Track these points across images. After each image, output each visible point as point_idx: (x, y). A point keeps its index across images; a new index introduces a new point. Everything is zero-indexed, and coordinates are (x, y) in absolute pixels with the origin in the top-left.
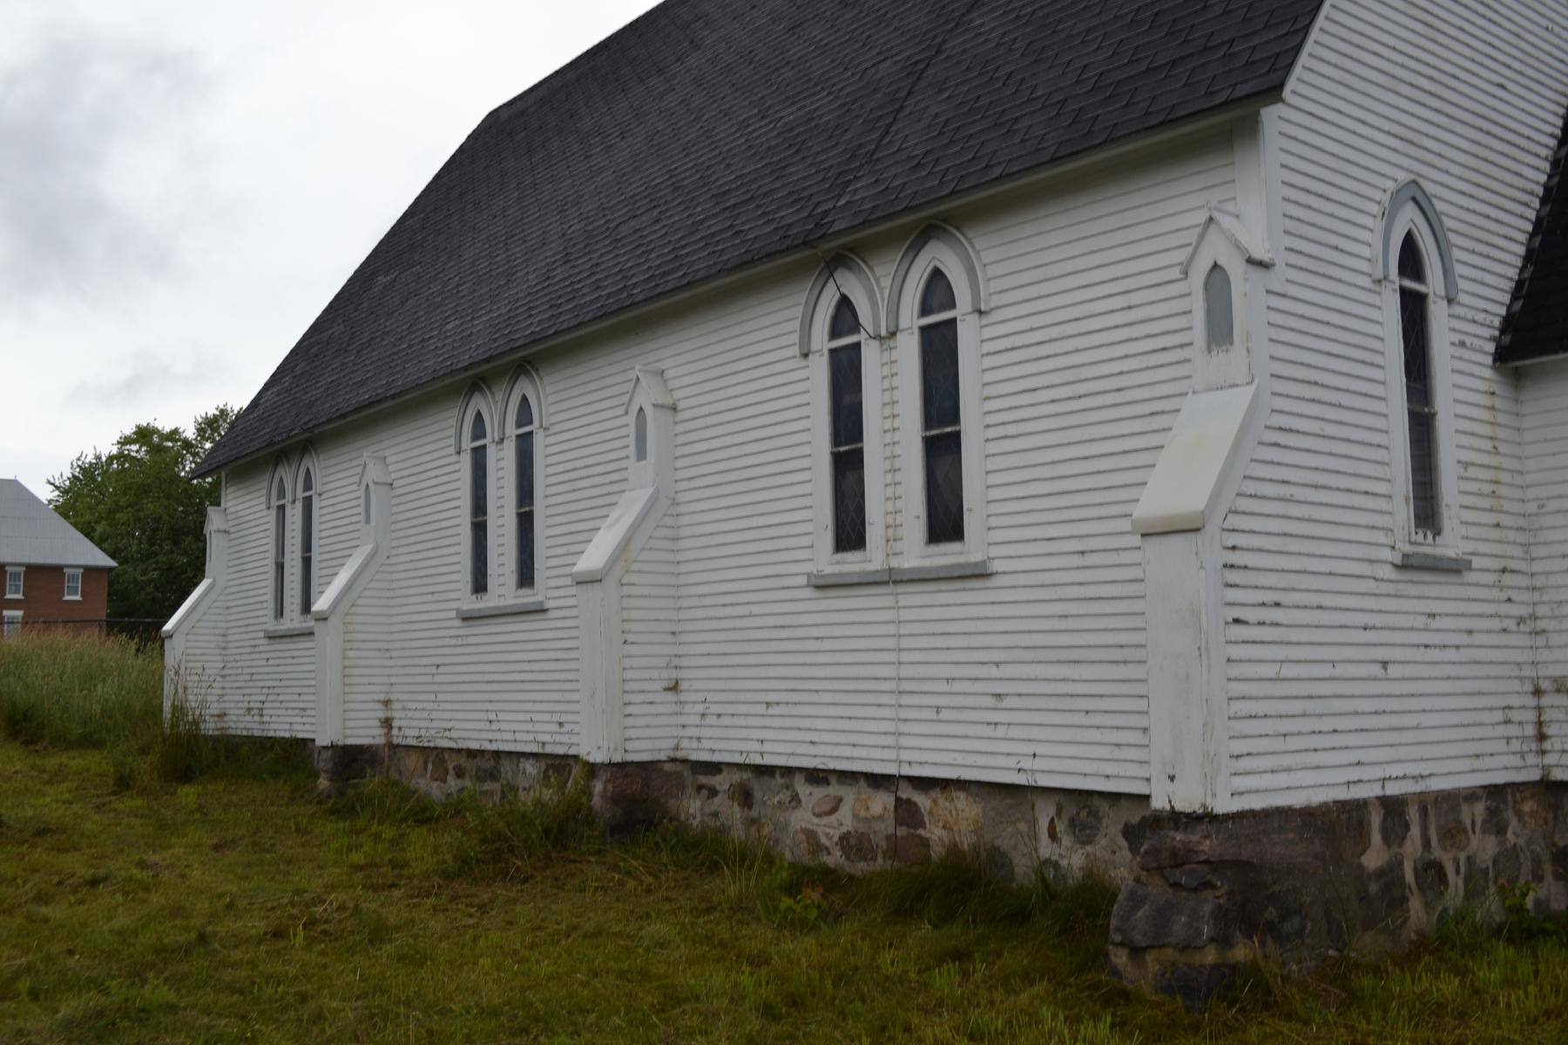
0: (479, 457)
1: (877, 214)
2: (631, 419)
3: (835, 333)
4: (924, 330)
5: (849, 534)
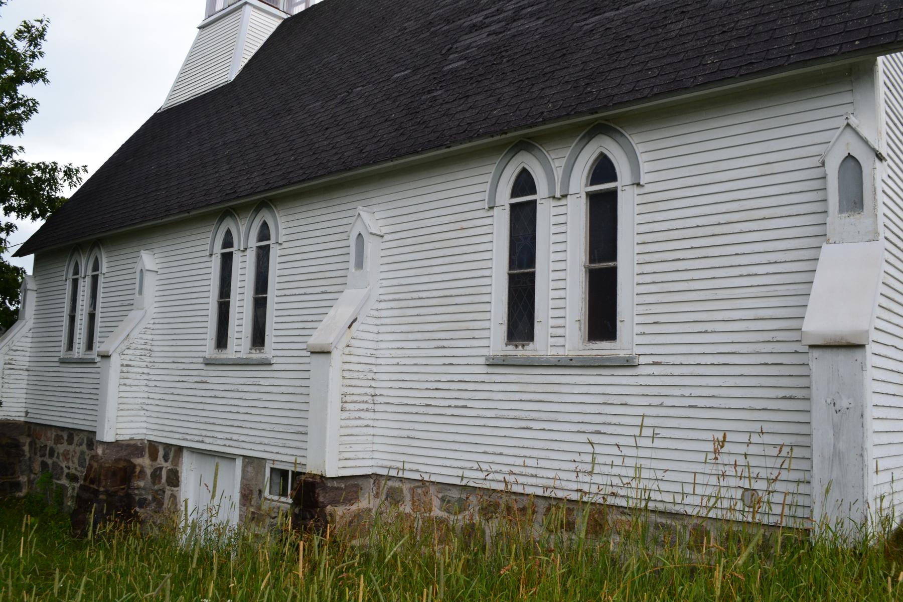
0: (227, 260)
1: (258, 190)
2: (352, 242)
3: (224, 247)
4: (512, 206)
5: (222, 341)
